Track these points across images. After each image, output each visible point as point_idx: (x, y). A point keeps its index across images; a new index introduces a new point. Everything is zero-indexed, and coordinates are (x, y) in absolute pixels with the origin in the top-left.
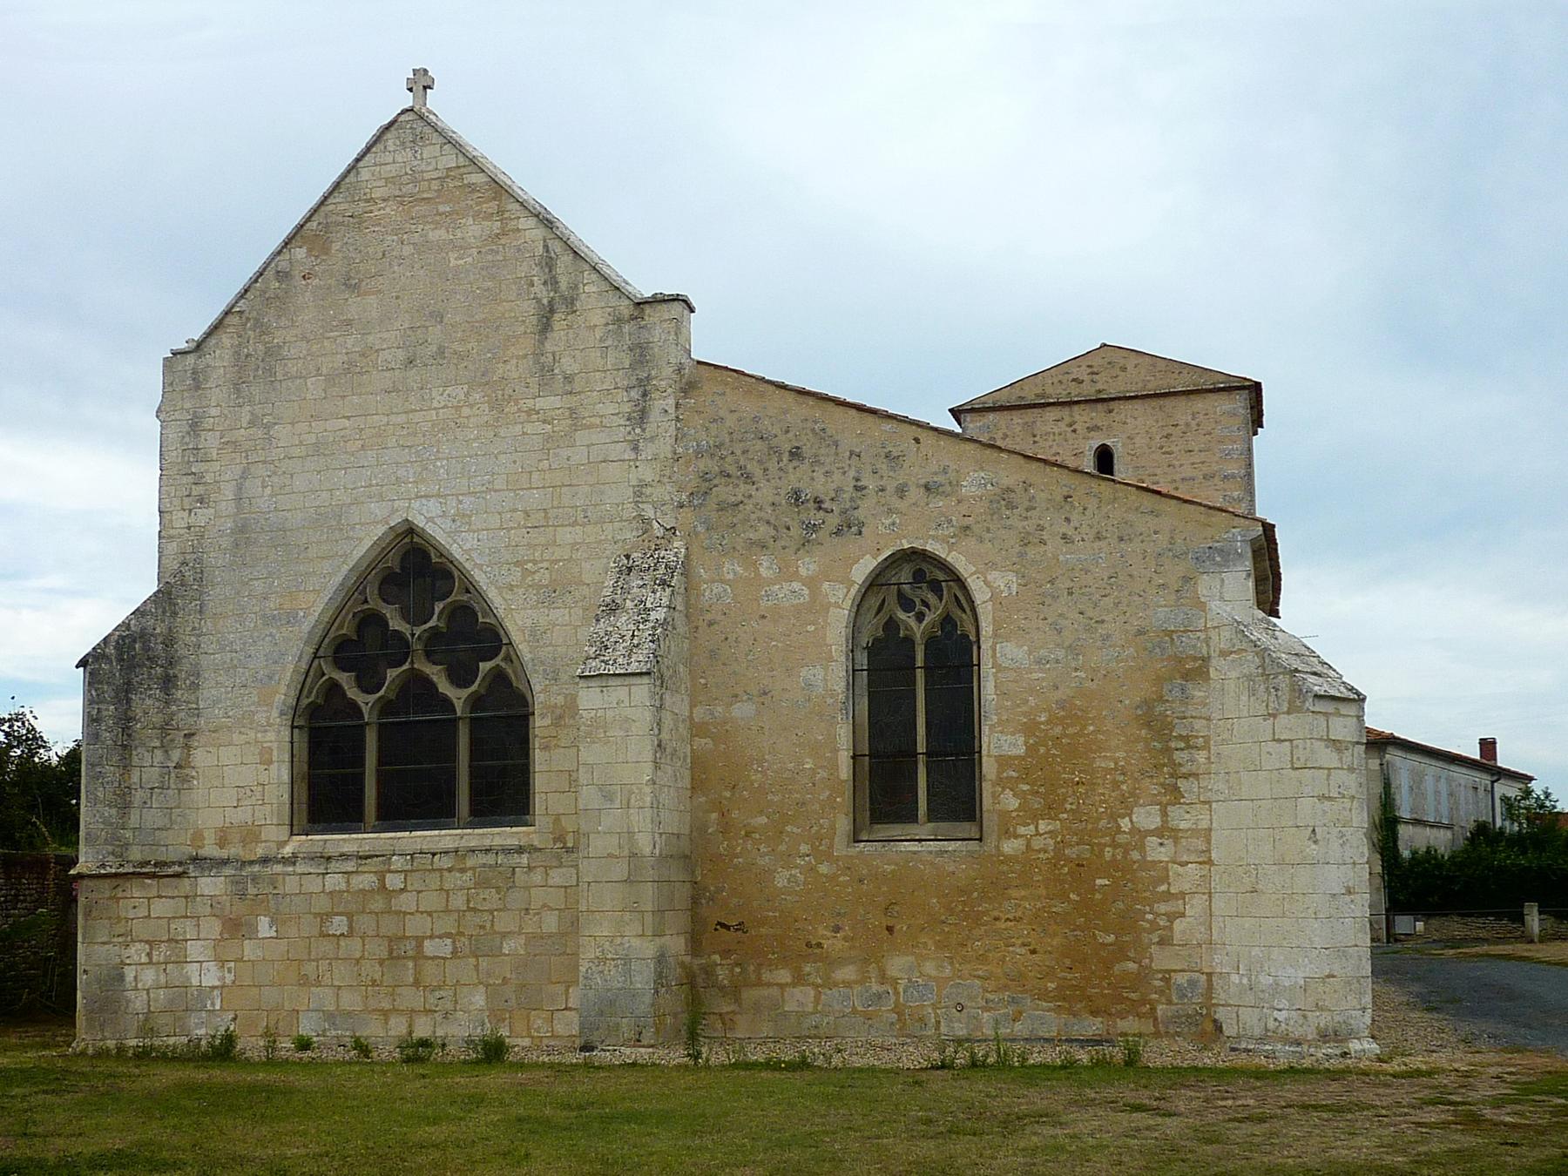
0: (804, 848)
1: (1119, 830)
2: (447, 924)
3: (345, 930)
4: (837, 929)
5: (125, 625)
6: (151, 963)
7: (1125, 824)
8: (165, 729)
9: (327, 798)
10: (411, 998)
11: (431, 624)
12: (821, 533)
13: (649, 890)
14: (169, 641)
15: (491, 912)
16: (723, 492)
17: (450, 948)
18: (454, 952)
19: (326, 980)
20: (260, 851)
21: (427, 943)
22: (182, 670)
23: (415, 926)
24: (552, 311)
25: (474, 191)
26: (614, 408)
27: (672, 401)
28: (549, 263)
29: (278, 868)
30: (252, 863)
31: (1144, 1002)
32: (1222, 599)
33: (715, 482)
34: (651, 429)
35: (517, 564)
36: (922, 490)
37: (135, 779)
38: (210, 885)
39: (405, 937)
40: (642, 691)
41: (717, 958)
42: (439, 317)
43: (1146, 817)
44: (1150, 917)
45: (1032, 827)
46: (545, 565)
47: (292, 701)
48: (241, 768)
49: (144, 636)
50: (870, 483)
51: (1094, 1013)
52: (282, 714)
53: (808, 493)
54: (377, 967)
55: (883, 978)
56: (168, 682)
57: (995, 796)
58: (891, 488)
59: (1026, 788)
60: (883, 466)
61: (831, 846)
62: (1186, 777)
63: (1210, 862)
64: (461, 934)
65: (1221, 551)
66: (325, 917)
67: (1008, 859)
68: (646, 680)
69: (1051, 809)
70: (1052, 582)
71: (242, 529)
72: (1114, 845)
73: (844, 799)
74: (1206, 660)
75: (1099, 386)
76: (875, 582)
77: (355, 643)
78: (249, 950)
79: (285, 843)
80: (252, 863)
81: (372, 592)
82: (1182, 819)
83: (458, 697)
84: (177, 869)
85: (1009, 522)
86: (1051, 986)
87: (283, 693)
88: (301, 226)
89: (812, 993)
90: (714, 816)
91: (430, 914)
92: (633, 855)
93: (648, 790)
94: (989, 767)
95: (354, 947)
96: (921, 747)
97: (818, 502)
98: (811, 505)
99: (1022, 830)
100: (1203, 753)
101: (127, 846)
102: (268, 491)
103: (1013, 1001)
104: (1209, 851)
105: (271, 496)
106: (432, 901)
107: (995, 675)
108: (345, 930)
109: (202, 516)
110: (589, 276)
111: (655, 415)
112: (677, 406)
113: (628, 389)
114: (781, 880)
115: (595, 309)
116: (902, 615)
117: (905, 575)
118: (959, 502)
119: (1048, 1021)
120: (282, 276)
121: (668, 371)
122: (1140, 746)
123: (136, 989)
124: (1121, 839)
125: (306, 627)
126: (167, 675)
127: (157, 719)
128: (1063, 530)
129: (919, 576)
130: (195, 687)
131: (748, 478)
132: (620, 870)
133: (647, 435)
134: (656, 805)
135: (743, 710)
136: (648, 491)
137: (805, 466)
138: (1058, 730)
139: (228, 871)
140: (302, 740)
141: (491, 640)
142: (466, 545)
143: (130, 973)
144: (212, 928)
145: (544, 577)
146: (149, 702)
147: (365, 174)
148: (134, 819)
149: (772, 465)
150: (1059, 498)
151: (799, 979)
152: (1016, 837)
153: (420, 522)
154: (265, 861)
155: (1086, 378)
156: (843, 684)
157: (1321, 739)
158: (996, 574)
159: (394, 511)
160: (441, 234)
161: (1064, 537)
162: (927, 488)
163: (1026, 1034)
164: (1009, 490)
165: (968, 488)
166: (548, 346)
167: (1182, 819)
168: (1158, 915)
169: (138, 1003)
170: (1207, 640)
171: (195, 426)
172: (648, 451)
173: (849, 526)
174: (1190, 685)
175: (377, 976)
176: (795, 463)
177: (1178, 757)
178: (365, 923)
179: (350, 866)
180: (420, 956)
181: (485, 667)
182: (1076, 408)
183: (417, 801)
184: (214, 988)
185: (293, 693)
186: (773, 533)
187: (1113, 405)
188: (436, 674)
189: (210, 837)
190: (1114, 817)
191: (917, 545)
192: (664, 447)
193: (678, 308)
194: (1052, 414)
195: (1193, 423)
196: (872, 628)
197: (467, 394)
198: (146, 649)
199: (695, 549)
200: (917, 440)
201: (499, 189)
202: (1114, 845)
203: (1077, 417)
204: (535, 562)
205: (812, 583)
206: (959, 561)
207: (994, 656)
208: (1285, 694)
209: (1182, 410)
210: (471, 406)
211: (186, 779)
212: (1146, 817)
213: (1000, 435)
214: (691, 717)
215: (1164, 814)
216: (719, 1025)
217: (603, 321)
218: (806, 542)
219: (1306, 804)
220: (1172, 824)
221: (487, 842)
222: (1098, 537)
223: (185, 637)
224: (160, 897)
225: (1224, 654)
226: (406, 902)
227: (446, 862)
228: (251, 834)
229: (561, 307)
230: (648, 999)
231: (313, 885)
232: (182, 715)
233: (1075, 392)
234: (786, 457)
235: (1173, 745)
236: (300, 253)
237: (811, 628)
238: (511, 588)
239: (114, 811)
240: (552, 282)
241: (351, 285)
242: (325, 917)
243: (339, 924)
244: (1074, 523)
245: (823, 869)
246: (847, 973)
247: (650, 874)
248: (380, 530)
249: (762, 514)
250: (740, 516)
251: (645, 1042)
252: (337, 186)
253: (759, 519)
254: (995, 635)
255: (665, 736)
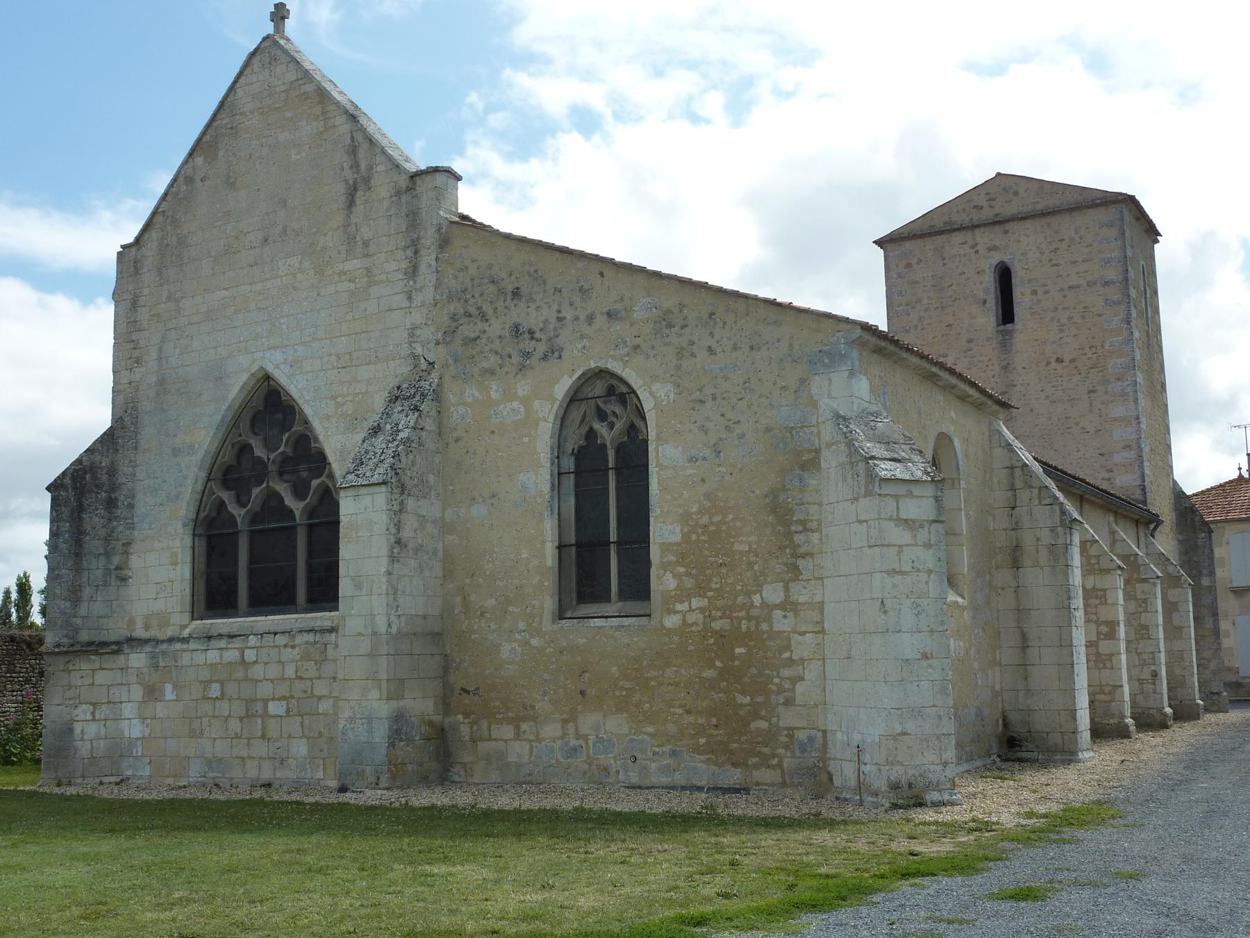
0: (522, 625)
1: (752, 606)
2: (282, 690)
3: (218, 694)
4: (545, 694)
5: (79, 461)
6: (94, 720)
7: (757, 599)
8: (107, 539)
9: (215, 595)
10: (260, 749)
11: (281, 450)
12: (533, 359)
13: (383, 662)
14: (112, 472)
15: (311, 679)
16: (468, 330)
17: (284, 708)
18: (288, 711)
19: (206, 734)
20: (170, 632)
21: (271, 705)
22: (121, 496)
23: (264, 690)
24: (355, 189)
25: (308, 98)
26: (393, 266)
27: (434, 256)
28: (353, 151)
29: (178, 646)
30: (163, 642)
31: (774, 756)
32: (829, 396)
33: (461, 321)
34: (420, 279)
35: (333, 398)
36: (606, 317)
37: (84, 579)
38: (137, 660)
39: (256, 700)
40: (381, 495)
41: (460, 717)
42: (283, 203)
43: (773, 593)
44: (777, 680)
45: (686, 604)
46: (350, 398)
47: (192, 515)
48: (159, 570)
49: (93, 469)
50: (568, 314)
51: (735, 765)
52: (185, 525)
53: (524, 327)
54: (239, 724)
55: (578, 736)
56: (111, 504)
57: (659, 578)
58: (582, 318)
59: (682, 570)
60: (577, 299)
61: (540, 623)
62: (803, 556)
63: (823, 631)
64: (292, 697)
65: (829, 353)
66: (206, 684)
67: (669, 632)
68: (383, 489)
69: (700, 590)
70: (700, 390)
71: (162, 382)
72: (749, 618)
73: (550, 583)
74: (818, 451)
75: (996, 210)
76: (574, 398)
77: (233, 471)
78: (160, 709)
79: (187, 626)
80: (163, 642)
81: (245, 425)
82: (801, 594)
83: (296, 507)
84: (114, 647)
85: (668, 340)
86: (702, 741)
87: (184, 509)
88: (199, 141)
89: (528, 747)
90: (459, 599)
91: (272, 681)
92: (375, 633)
93: (384, 579)
94: (655, 553)
95: (224, 708)
96: (613, 537)
97: (531, 332)
98: (526, 336)
99: (679, 607)
100: (816, 535)
101: (77, 630)
102: (177, 351)
103: (674, 754)
104: (823, 622)
105: (180, 354)
106: (274, 671)
107: (658, 473)
108: (218, 694)
109: (139, 372)
110: (380, 158)
111: (423, 269)
112: (437, 259)
113: (406, 248)
114: (505, 653)
115: (382, 189)
116: (597, 426)
117: (599, 388)
118: (632, 325)
119: (702, 770)
120: (189, 180)
121: (431, 231)
122: (768, 531)
123: (82, 740)
124: (755, 612)
125: (200, 454)
126: (110, 498)
127: (103, 532)
128: (709, 344)
129: (611, 391)
130: (131, 506)
131: (484, 317)
132: (365, 647)
133: (418, 286)
134: (394, 591)
135: (479, 511)
136: (418, 332)
137: (522, 304)
138: (705, 520)
139: (148, 648)
140: (202, 545)
141: (319, 462)
142: (296, 386)
143: (78, 728)
144: (137, 692)
145: (349, 408)
146: (96, 519)
147: (240, 93)
148: (83, 609)
149: (500, 305)
150: (705, 316)
151: (518, 736)
152: (675, 612)
153: (270, 369)
154: (171, 640)
155: (985, 204)
156: (548, 486)
157: (890, 519)
158: (658, 385)
159: (254, 361)
160: (284, 136)
161: (710, 349)
162: (609, 314)
163: (683, 783)
164: (669, 311)
165: (639, 314)
166: (353, 219)
167: (801, 594)
168: (782, 679)
169: (84, 749)
170: (819, 434)
171: (134, 305)
172: (419, 298)
173: (553, 352)
174: (806, 475)
175: (239, 731)
176: (516, 301)
177: (798, 539)
178: (231, 689)
179: (223, 643)
180: (265, 715)
181: (315, 483)
182: (978, 232)
183: (273, 595)
184: (137, 739)
185: (193, 509)
186: (500, 361)
187: (1009, 226)
188: (283, 489)
189: (139, 623)
190: (749, 594)
191: (601, 364)
192: (428, 295)
193: (440, 179)
194: (958, 238)
195: (1077, 237)
196: (575, 440)
197: (301, 263)
198: (95, 478)
199: (447, 379)
200: (602, 274)
201: (322, 95)
202: (749, 618)
203: (978, 240)
204: (343, 396)
205: (526, 401)
206: (631, 376)
207: (657, 456)
208: (862, 479)
209: (1066, 226)
210: (303, 273)
211: (123, 579)
212: (773, 593)
213: (916, 260)
214: (443, 518)
215: (787, 590)
216: (462, 773)
217: (388, 194)
218: (522, 368)
219: (877, 577)
220: (793, 598)
221: (311, 625)
222: (735, 348)
223: (124, 469)
224: (102, 669)
225: (829, 445)
226: (257, 672)
227: (281, 640)
228: (164, 621)
229: (361, 186)
230: (384, 751)
231: (200, 658)
232: (120, 529)
233: (977, 217)
234: (509, 296)
235: (793, 528)
236: (199, 160)
237: (526, 440)
238: (328, 417)
239: (68, 604)
240: (355, 166)
241: (230, 184)
242: (206, 684)
243: (215, 690)
244: (717, 337)
245: (535, 642)
246: (551, 730)
247: (384, 649)
248: (244, 377)
249: (492, 346)
250: (478, 349)
251: (381, 785)
252: (222, 105)
253: (491, 351)
254: (658, 439)
255: (406, 534)
